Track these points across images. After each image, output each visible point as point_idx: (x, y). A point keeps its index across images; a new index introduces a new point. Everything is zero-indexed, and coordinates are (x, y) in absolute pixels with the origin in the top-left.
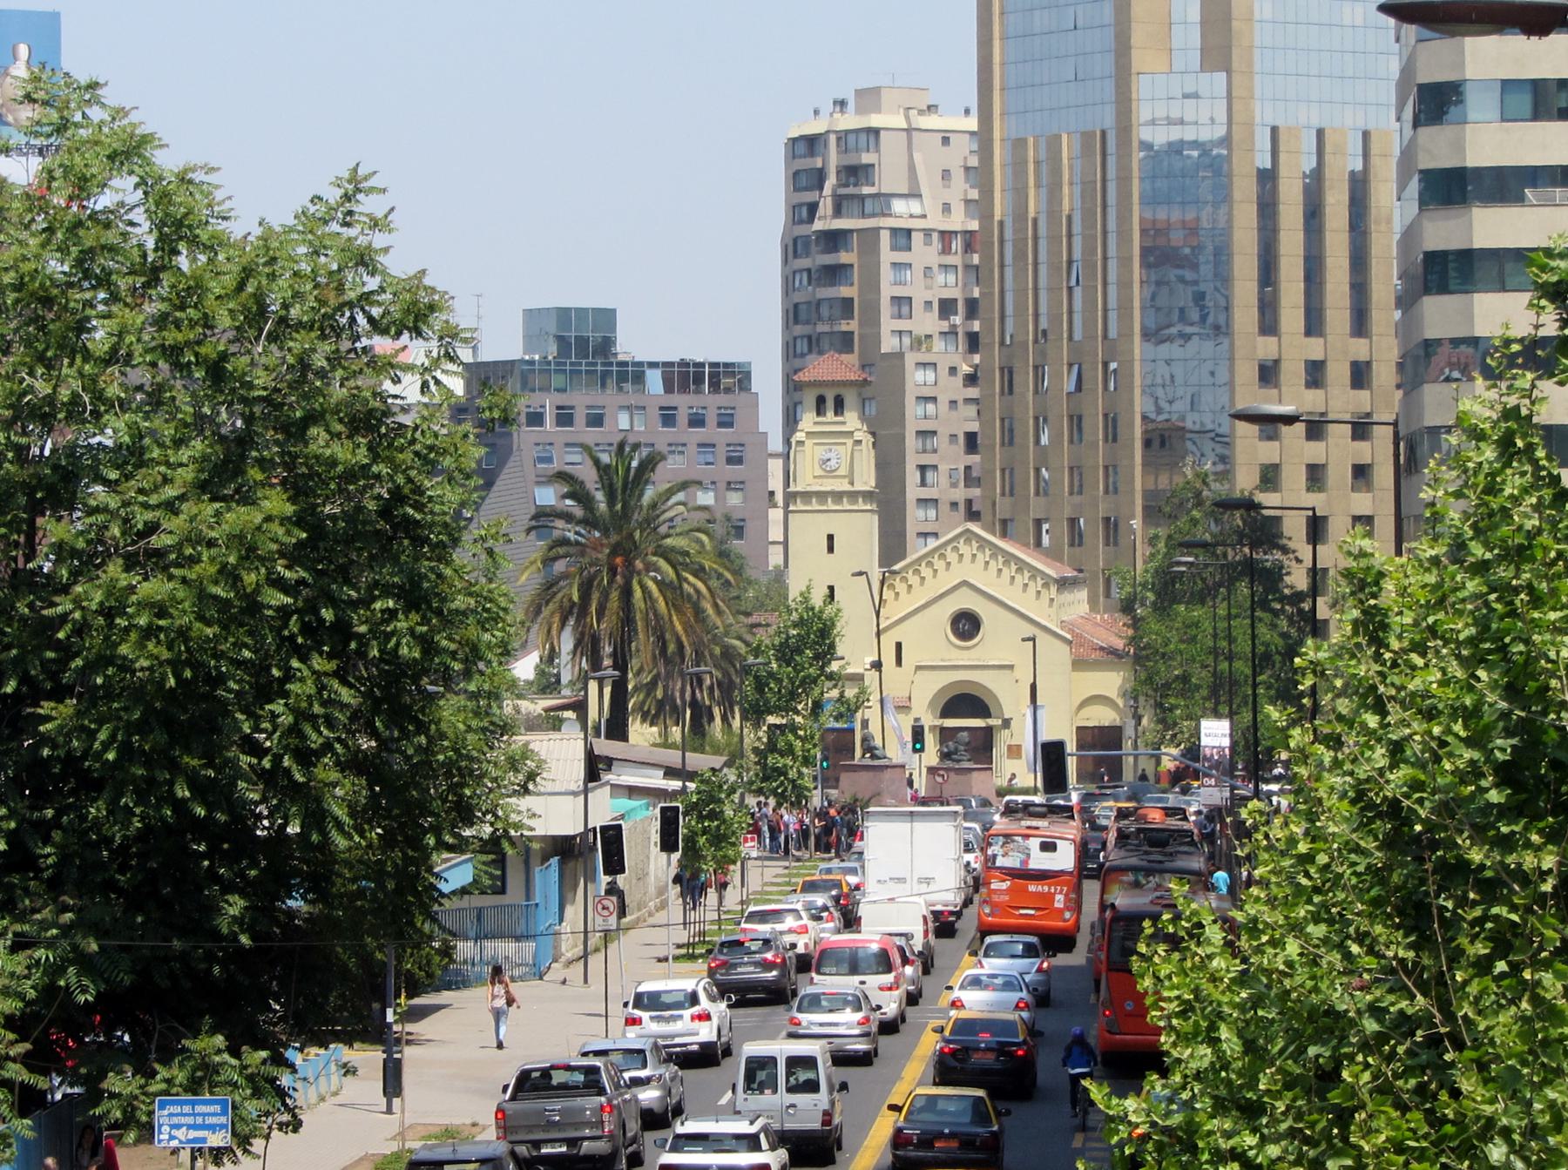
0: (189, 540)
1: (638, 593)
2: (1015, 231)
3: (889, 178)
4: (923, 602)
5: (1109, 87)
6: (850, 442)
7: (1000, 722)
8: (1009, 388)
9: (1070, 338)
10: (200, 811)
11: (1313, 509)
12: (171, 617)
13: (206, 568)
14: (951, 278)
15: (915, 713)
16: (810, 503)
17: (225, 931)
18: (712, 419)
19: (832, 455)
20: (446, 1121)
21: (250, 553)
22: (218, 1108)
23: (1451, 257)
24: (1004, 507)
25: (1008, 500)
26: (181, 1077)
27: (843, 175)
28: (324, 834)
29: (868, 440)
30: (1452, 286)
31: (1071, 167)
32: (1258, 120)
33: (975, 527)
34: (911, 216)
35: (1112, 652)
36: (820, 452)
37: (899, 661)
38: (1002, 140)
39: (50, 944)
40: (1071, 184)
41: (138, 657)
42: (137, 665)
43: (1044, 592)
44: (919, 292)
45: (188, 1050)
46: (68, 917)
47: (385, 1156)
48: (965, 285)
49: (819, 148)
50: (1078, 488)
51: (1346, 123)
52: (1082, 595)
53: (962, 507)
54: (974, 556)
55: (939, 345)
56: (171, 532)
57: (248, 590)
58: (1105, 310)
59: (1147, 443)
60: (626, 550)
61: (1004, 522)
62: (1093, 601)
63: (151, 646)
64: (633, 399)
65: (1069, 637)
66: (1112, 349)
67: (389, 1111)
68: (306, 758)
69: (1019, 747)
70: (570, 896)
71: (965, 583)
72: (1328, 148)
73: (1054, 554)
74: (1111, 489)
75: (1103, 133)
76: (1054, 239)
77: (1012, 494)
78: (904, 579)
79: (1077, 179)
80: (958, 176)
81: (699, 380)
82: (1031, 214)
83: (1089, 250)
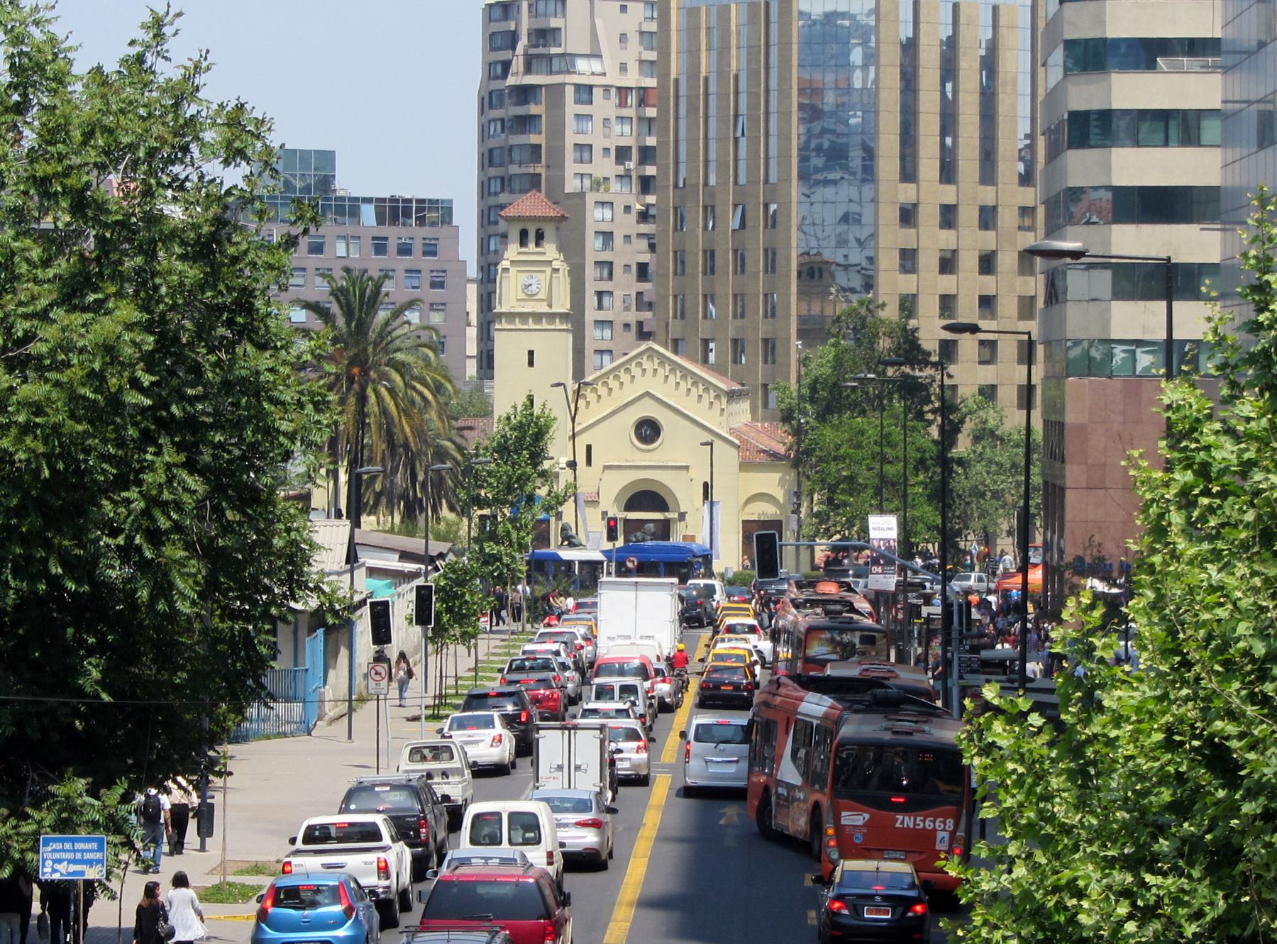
0: (61, 347)
1: (372, 398)
2: (689, 88)
4: (610, 410)
6: (548, 270)
7: (676, 515)
8: (679, 226)
9: (736, 183)
11: (1029, 333)
12: (47, 415)
14: (627, 128)
15: (602, 507)
16: (514, 323)
17: (88, 689)
18: (418, 248)
19: (533, 281)
22: (95, 845)
23: (1093, 117)
24: (676, 328)
25: (678, 322)
26: (49, 819)
27: (533, 37)
28: (171, 604)
29: (564, 268)
31: (738, 33)
33: (651, 344)
34: (593, 74)
35: (774, 456)
36: (523, 278)
37: (589, 462)
38: (679, 9)
40: (738, 48)
41: (17, 451)
42: (16, 457)
43: (716, 402)
45: (54, 795)
47: (207, 888)
49: (513, 11)
50: (741, 314)
52: (745, 405)
53: (634, 328)
54: (655, 370)
55: (615, 186)
56: (46, 341)
57: (113, 390)
58: (767, 158)
62: (753, 410)
63: (28, 440)
65: (737, 442)
66: (773, 192)
68: (156, 538)
70: (332, 662)
71: (647, 394)
72: (962, 20)
73: (719, 369)
74: (771, 313)
76: (723, 96)
77: (683, 317)
79: (744, 42)
80: (634, 39)
81: (407, 213)
82: (703, 73)
83: (753, 106)
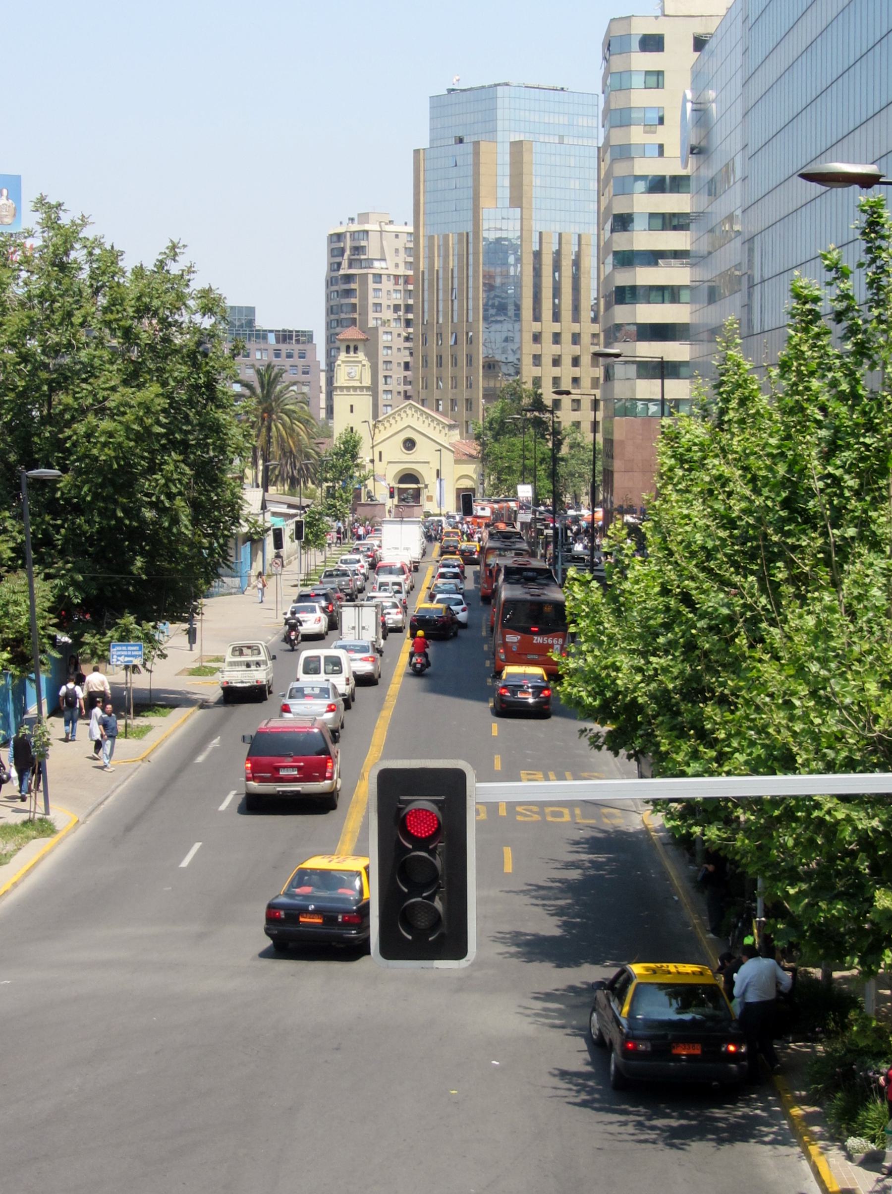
1: (274, 429)
2: (429, 275)
3: (372, 252)
5: (470, 214)
6: (360, 365)
9: (452, 321)
10: (127, 522)
13: (129, 417)
14: (398, 296)
18: (296, 355)
20: (216, 654)
21: (148, 410)
22: (137, 648)
25: (425, 391)
30: (627, 301)
31: (453, 248)
32: (534, 229)
33: (411, 401)
35: (471, 456)
36: (348, 369)
37: (380, 460)
39: (62, 577)
44: (385, 302)
46: (69, 566)
48: (405, 298)
51: (571, 231)
53: (402, 394)
55: (393, 324)
58: (467, 310)
59: (483, 367)
60: (269, 411)
61: (423, 400)
62: (461, 434)
63: (106, 450)
64: (262, 346)
67: (191, 650)
68: (171, 497)
69: (431, 497)
71: (409, 426)
73: (444, 414)
74: (470, 386)
75: (467, 234)
76: (446, 279)
78: (383, 424)
79: (456, 252)
80: (402, 251)
81: (291, 338)
82: (436, 268)
83: (460, 284)
